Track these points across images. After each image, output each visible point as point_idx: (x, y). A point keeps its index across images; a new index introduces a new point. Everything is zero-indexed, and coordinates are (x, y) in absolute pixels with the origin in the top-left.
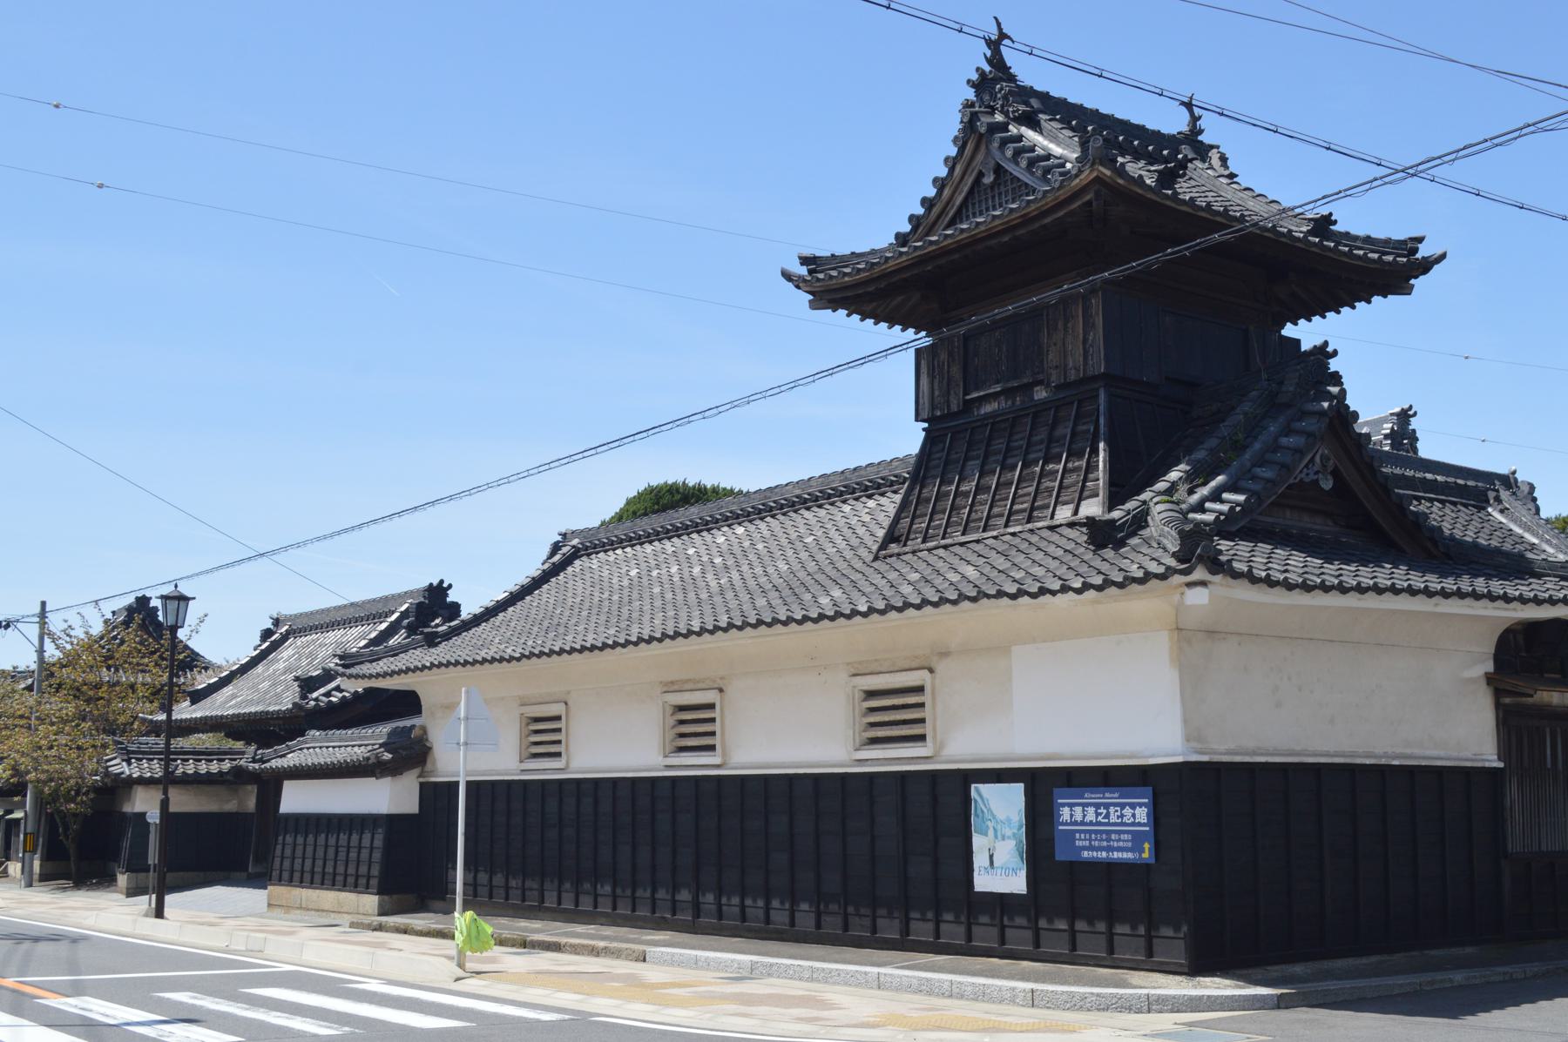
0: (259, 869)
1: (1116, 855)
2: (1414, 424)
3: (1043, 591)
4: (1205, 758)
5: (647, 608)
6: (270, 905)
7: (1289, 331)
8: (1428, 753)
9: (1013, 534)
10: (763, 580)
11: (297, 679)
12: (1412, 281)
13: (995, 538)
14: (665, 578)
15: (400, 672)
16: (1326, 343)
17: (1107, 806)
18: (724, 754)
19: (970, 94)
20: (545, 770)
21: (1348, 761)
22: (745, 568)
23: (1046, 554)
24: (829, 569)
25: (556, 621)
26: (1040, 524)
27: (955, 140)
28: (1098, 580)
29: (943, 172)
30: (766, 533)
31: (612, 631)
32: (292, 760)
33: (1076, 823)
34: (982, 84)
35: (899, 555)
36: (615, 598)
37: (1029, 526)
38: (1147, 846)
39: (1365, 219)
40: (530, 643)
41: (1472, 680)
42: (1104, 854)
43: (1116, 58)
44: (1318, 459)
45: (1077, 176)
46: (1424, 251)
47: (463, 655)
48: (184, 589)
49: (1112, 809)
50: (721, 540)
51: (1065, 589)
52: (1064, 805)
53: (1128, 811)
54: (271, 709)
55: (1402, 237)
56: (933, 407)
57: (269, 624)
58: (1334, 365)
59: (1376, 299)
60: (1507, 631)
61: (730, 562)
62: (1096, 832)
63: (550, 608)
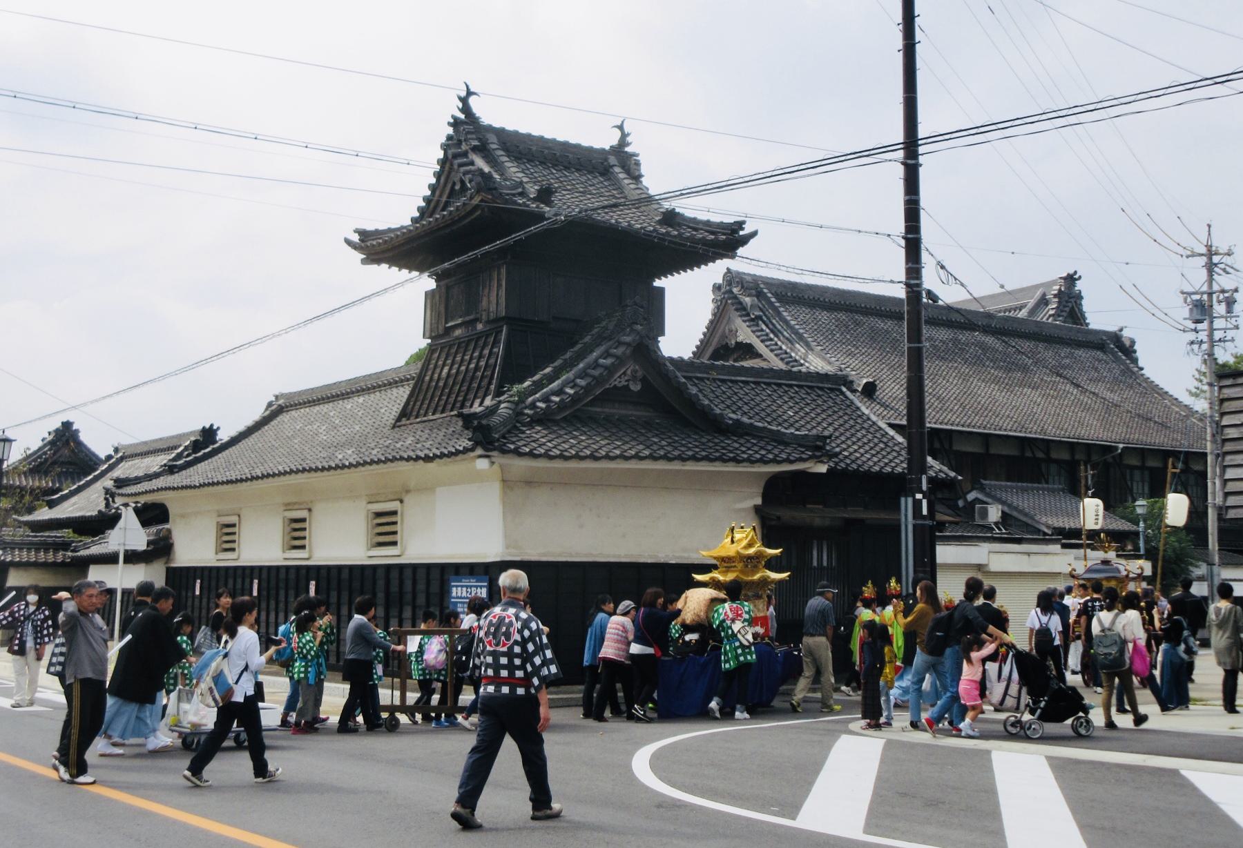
2: (1079, 286)
15: (154, 491)
18: (310, 551)
20: (385, 557)
29: (434, 181)
32: (95, 550)
41: (743, 510)
44: (629, 372)
47: (186, 482)
56: (431, 331)
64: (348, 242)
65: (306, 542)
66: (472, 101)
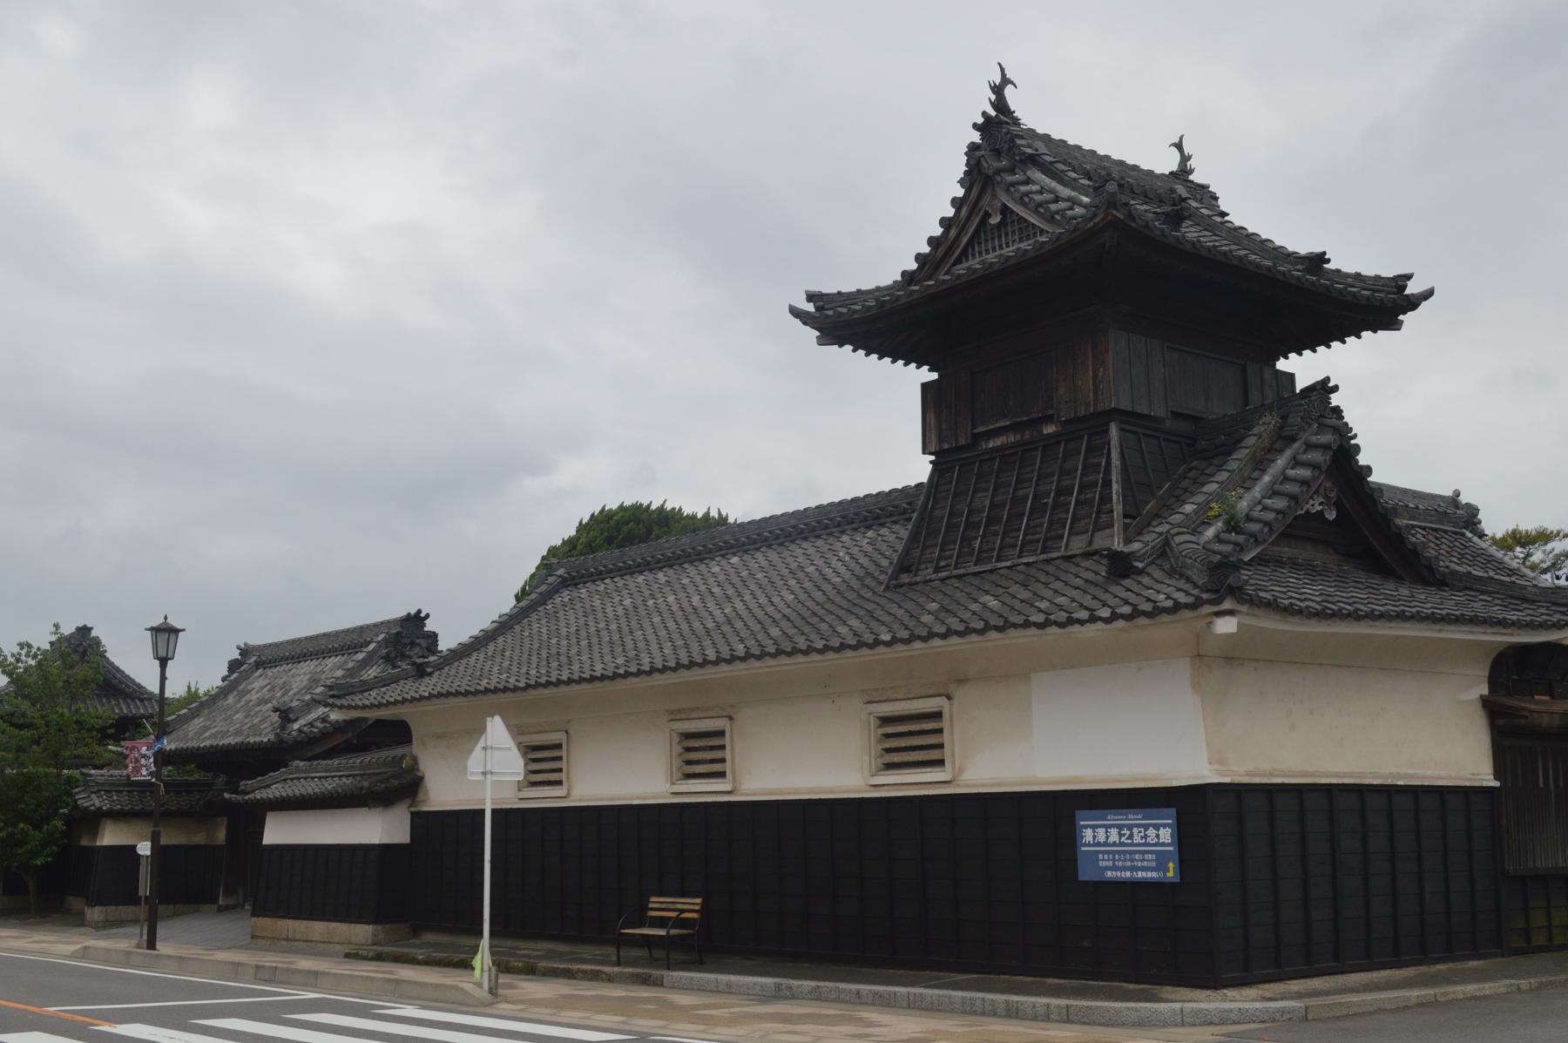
0: (230, 901)
1: (1140, 874)
3: (1071, 621)
4: (1227, 780)
5: (651, 637)
6: (253, 937)
8: (1429, 773)
9: (1028, 564)
10: (770, 609)
11: (276, 710)
13: (1009, 568)
14: (663, 607)
16: (1328, 379)
17: (1130, 827)
19: (976, 137)
20: (546, 798)
21: (1357, 781)
22: (747, 597)
23: (1066, 583)
24: (838, 599)
25: (554, 651)
26: (1054, 555)
28: (1127, 610)
30: (764, 563)
31: (620, 661)
32: (277, 791)
33: (1099, 844)
34: (987, 127)
35: (911, 584)
36: (613, 627)
37: (1044, 556)
38: (1171, 865)
40: (533, 672)
42: (1128, 874)
46: (1412, 288)
48: (174, 622)
49: (1135, 830)
50: (716, 569)
51: (1093, 619)
52: (1086, 827)
53: (1151, 832)
54: (251, 740)
56: (940, 441)
57: (236, 655)
58: (1335, 400)
60: (1499, 655)
61: (730, 592)
62: (1119, 852)
63: (545, 637)
64: (796, 312)
65: (563, 776)
66: (1009, 92)
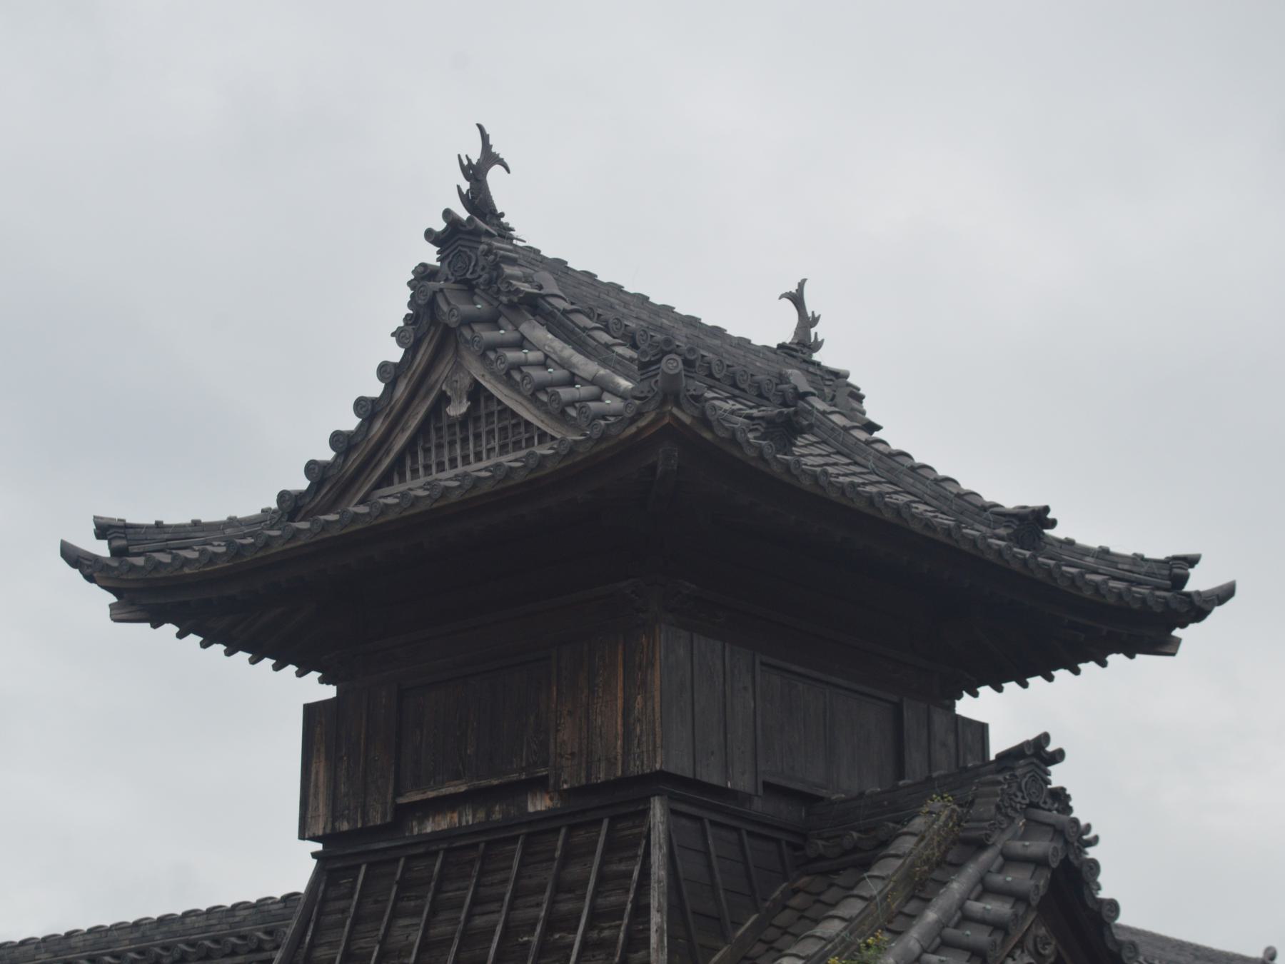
7: (330, 692)
12: (1177, 632)
16: (1045, 738)
27: (398, 335)
34: (450, 238)
39: (1101, 519)
43: (687, 225)
45: (633, 420)
46: (1198, 582)
55: (1161, 556)
56: (335, 816)
58: (1058, 776)
59: (1114, 659)
66: (494, 176)
